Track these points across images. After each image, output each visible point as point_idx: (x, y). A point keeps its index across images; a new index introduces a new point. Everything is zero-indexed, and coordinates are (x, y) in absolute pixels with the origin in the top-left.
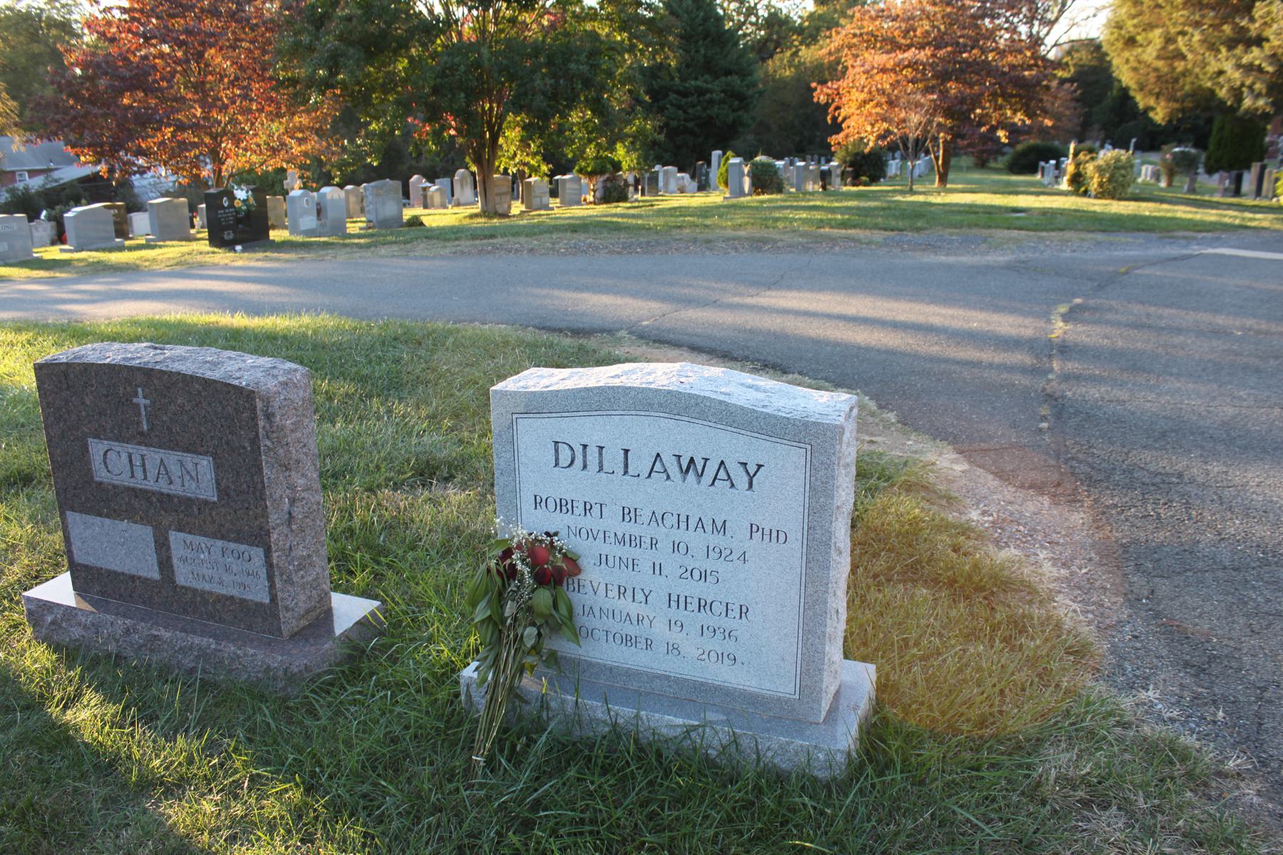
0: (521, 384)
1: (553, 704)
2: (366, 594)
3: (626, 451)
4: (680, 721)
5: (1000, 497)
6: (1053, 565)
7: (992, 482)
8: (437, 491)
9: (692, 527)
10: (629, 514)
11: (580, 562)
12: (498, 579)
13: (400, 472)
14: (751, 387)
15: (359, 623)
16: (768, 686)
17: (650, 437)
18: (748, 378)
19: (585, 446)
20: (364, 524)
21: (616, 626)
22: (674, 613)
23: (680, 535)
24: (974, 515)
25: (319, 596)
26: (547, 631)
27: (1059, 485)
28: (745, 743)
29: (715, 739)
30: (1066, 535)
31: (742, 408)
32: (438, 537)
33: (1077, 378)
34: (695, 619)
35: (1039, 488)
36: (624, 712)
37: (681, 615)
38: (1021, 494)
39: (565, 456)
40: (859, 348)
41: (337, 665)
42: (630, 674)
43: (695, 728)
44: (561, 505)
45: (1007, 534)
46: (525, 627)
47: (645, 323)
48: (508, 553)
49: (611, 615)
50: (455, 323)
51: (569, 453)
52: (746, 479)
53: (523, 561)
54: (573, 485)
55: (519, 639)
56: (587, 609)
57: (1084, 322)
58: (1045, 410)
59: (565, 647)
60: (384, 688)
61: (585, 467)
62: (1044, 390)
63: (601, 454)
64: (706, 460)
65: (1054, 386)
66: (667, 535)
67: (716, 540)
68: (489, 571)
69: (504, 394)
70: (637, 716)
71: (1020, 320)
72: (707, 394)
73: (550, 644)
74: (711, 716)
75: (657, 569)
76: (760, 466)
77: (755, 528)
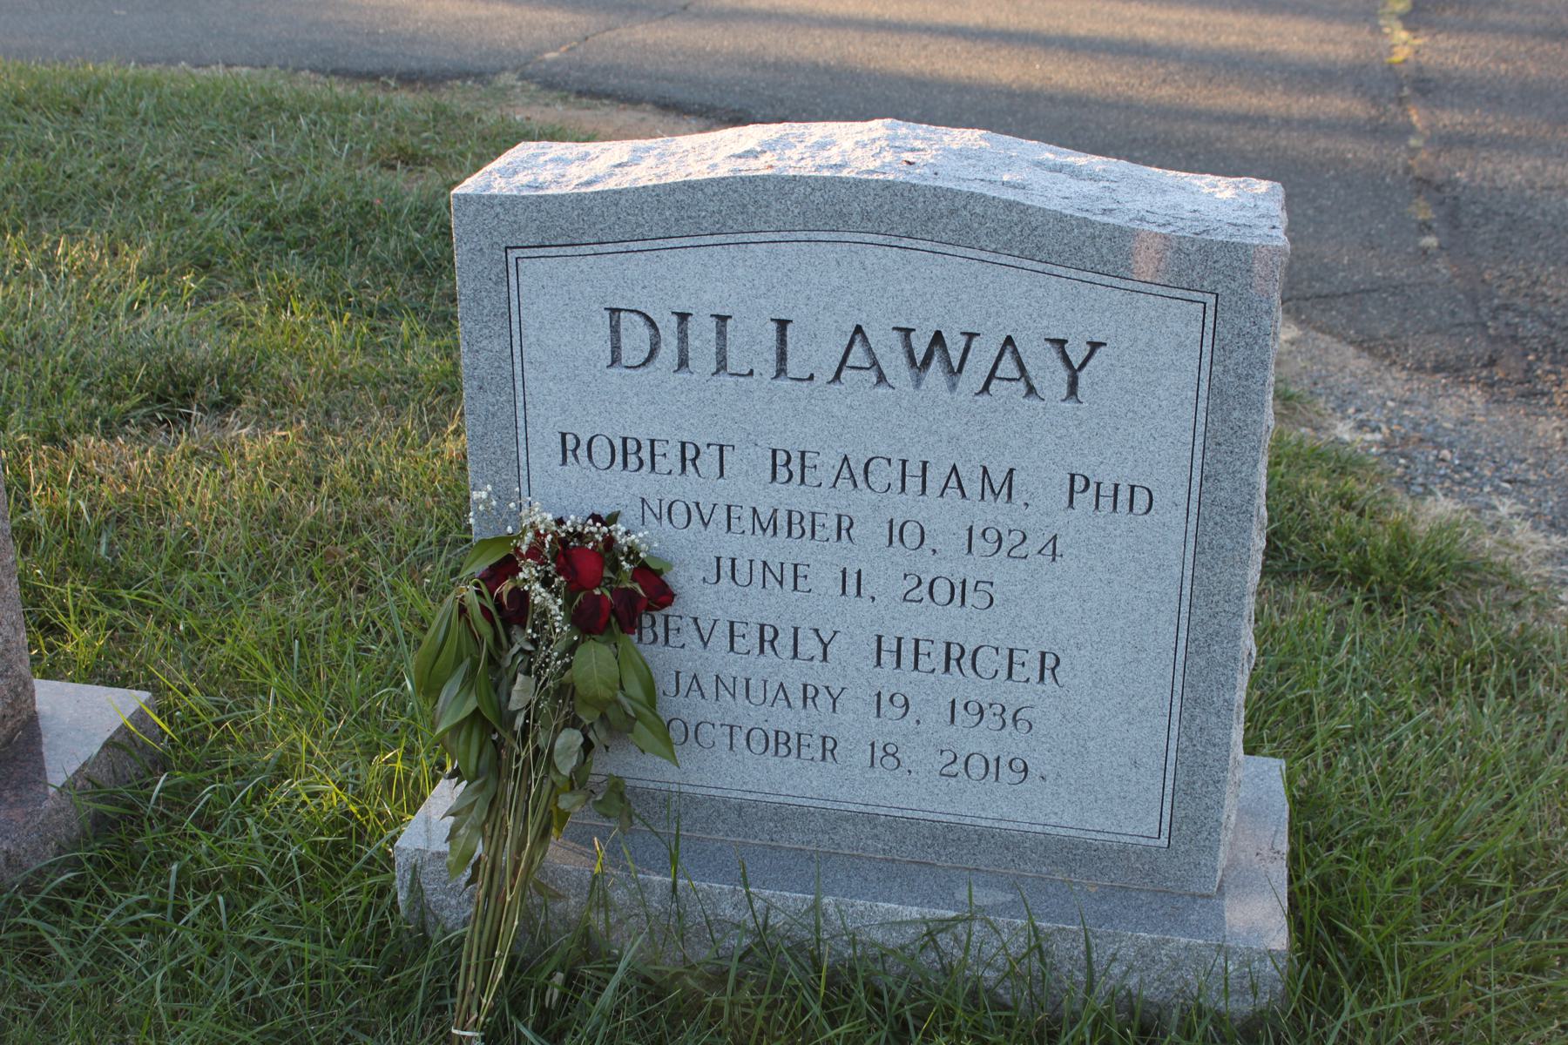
0: (523, 178)
1: (619, 896)
2: (101, 674)
3: (782, 324)
4: (913, 912)
5: (1380, 390)
6: (1535, 528)
7: (1360, 363)
8: (202, 430)
9: (934, 485)
10: (786, 465)
11: (669, 577)
12: (483, 627)
13: (112, 396)
14: (1059, 169)
15: (109, 744)
16: (1099, 822)
17: (843, 286)
18: (1048, 153)
19: (683, 317)
20: (56, 517)
21: (747, 713)
22: (888, 679)
23: (905, 506)
24: (1343, 430)
25: (13, 690)
26: (603, 735)
27: (1492, 362)
28: (1065, 951)
29: (993, 942)
30: (1536, 466)
31: (1060, 217)
32: (238, 534)
33: (1469, 142)
34: (932, 688)
35: (1454, 369)
36: (785, 903)
37: (905, 681)
38: (1422, 384)
39: (635, 338)
40: (1011, 94)
41: (75, 845)
42: (783, 815)
43: (946, 925)
44: (626, 452)
45: (1421, 468)
46: (557, 732)
47: (550, 56)
48: (506, 567)
49: (740, 690)
50: (143, 62)
51: (645, 332)
52: (1063, 374)
53: (546, 582)
54: (657, 405)
55: (544, 757)
56: (685, 681)
57: (1446, 28)
58: (1422, 210)
59: (639, 767)
60: (203, 886)
61: (683, 363)
62: (1408, 170)
63: (721, 333)
64: (971, 336)
65: (1424, 159)
66: (876, 508)
67: (992, 513)
68: (463, 610)
69: (486, 203)
70: (815, 907)
71: (1320, 29)
72: (977, 188)
73: (605, 765)
74: (983, 897)
75: (852, 583)
76: (1095, 346)
77: (1079, 483)
